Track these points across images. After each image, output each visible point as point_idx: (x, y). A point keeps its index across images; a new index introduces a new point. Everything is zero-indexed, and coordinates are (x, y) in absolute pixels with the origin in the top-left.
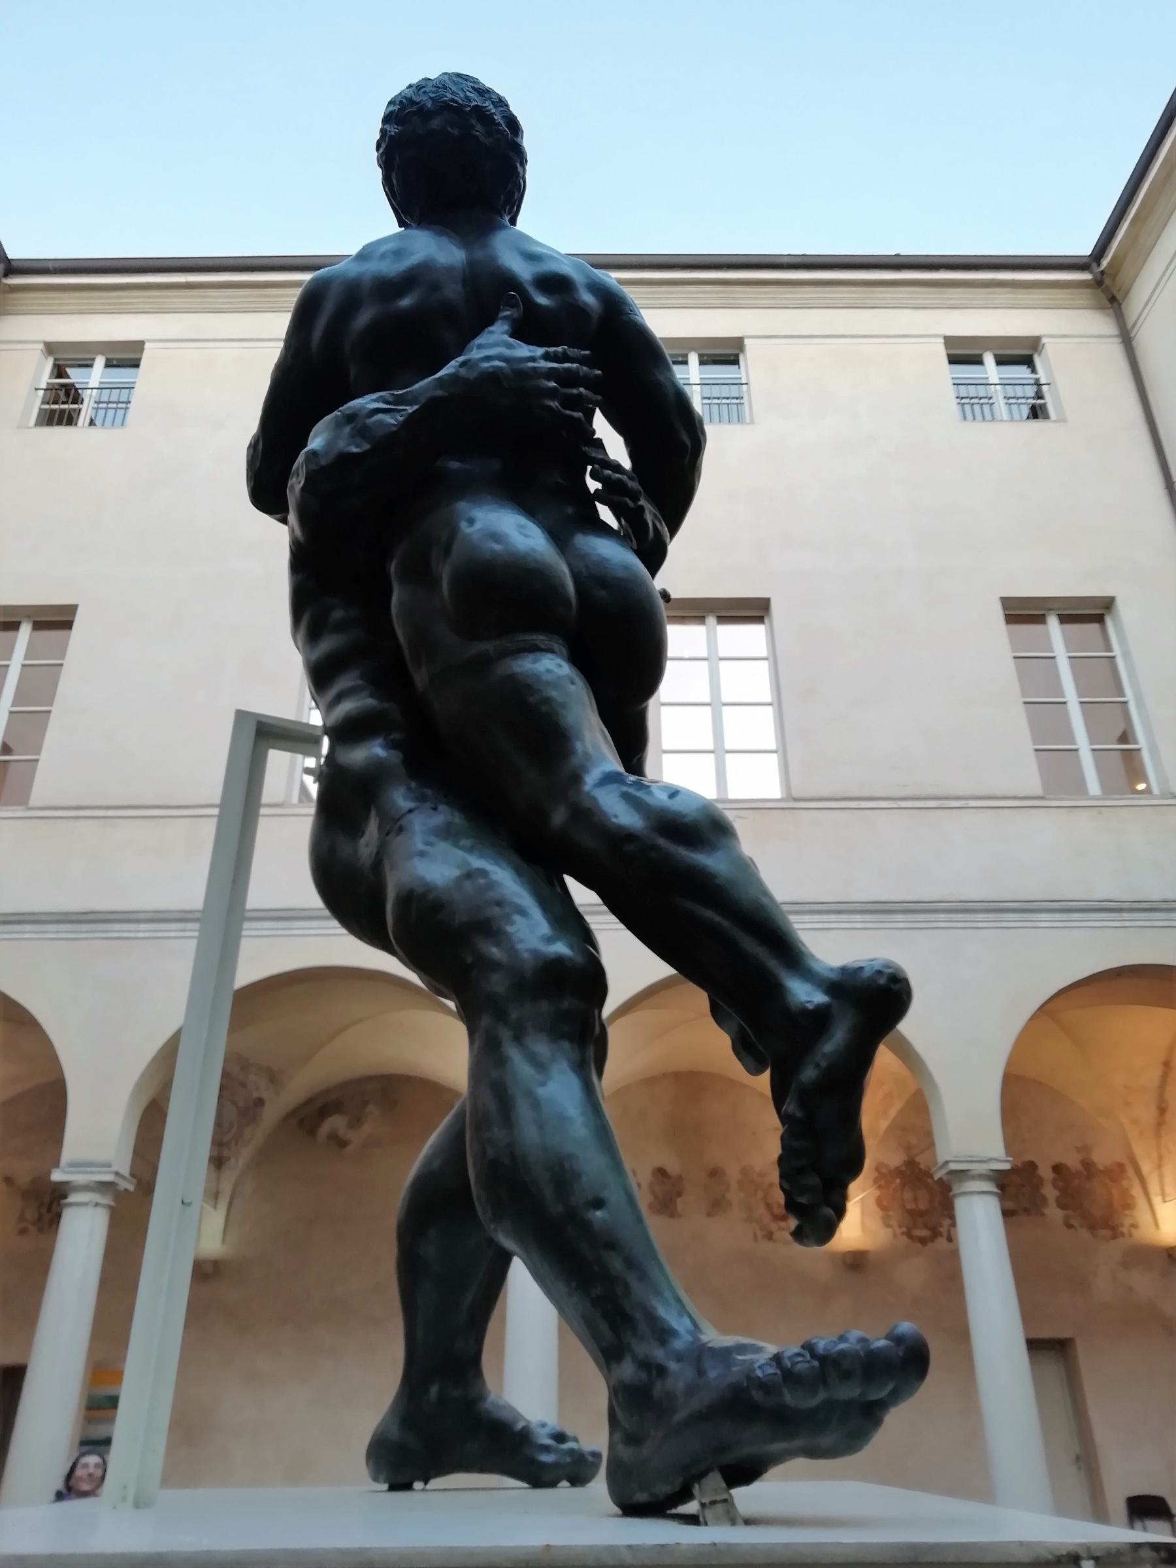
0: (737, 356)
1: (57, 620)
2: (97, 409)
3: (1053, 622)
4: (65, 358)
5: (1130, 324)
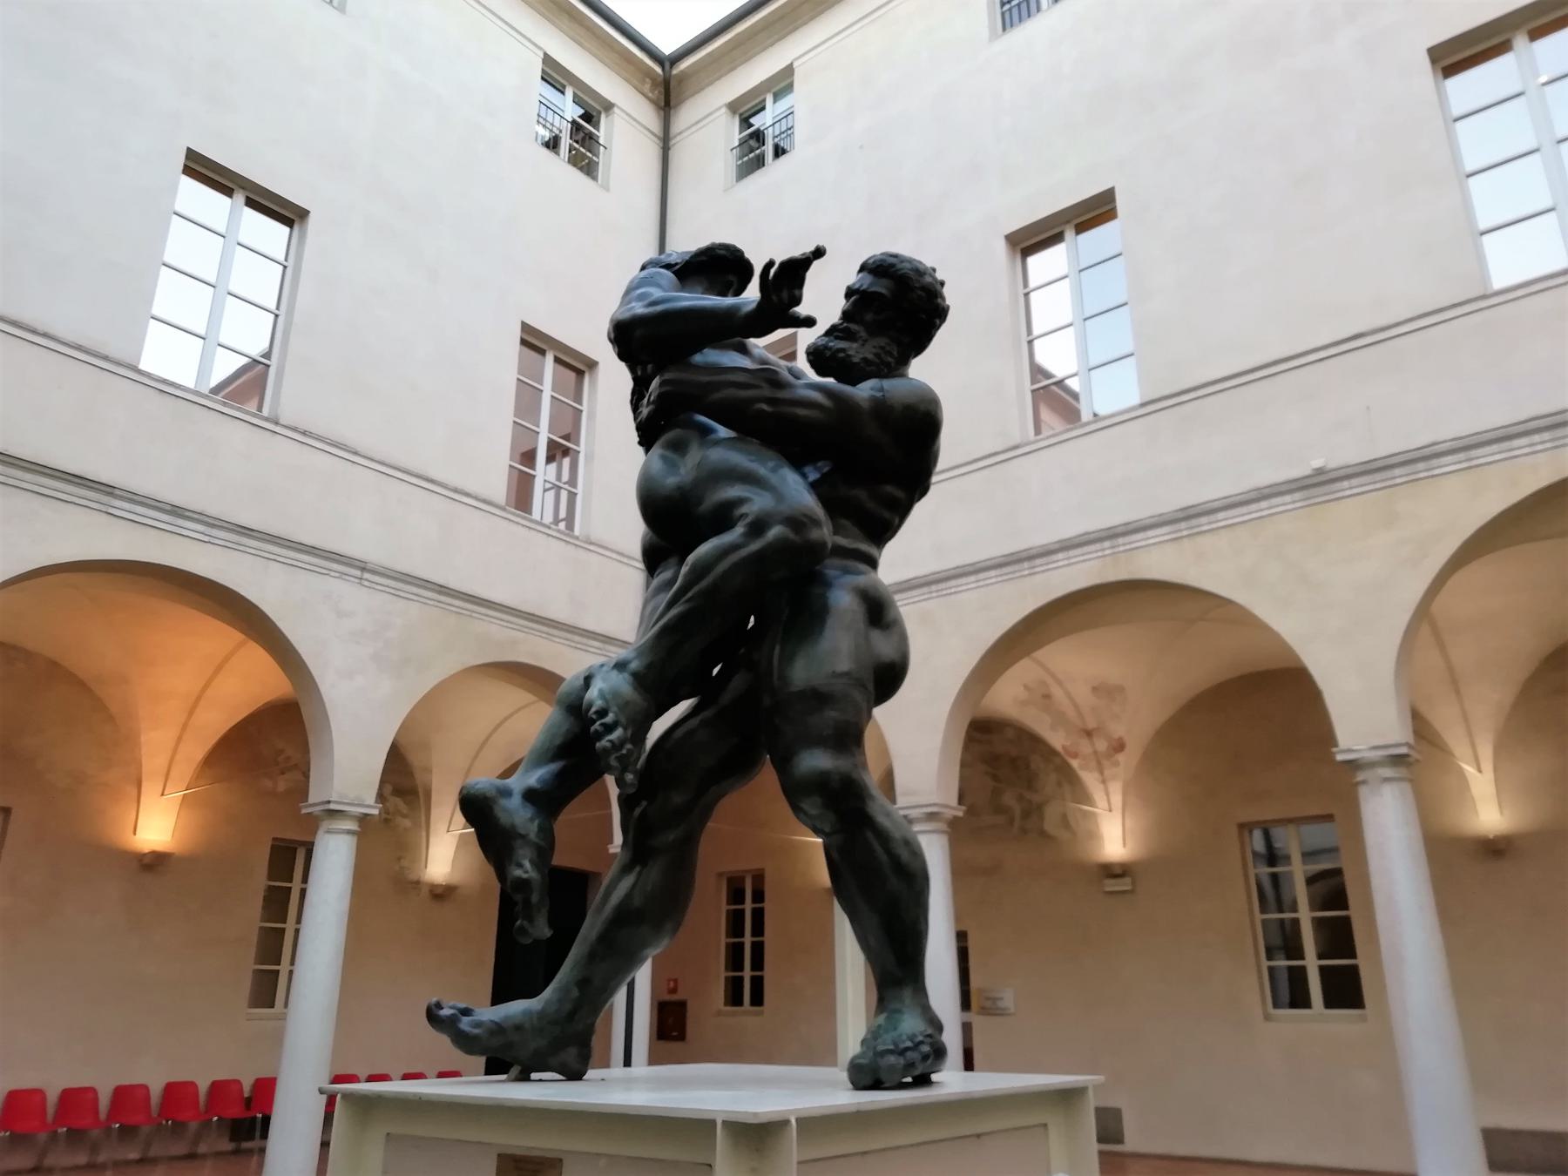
5: (674, 129)
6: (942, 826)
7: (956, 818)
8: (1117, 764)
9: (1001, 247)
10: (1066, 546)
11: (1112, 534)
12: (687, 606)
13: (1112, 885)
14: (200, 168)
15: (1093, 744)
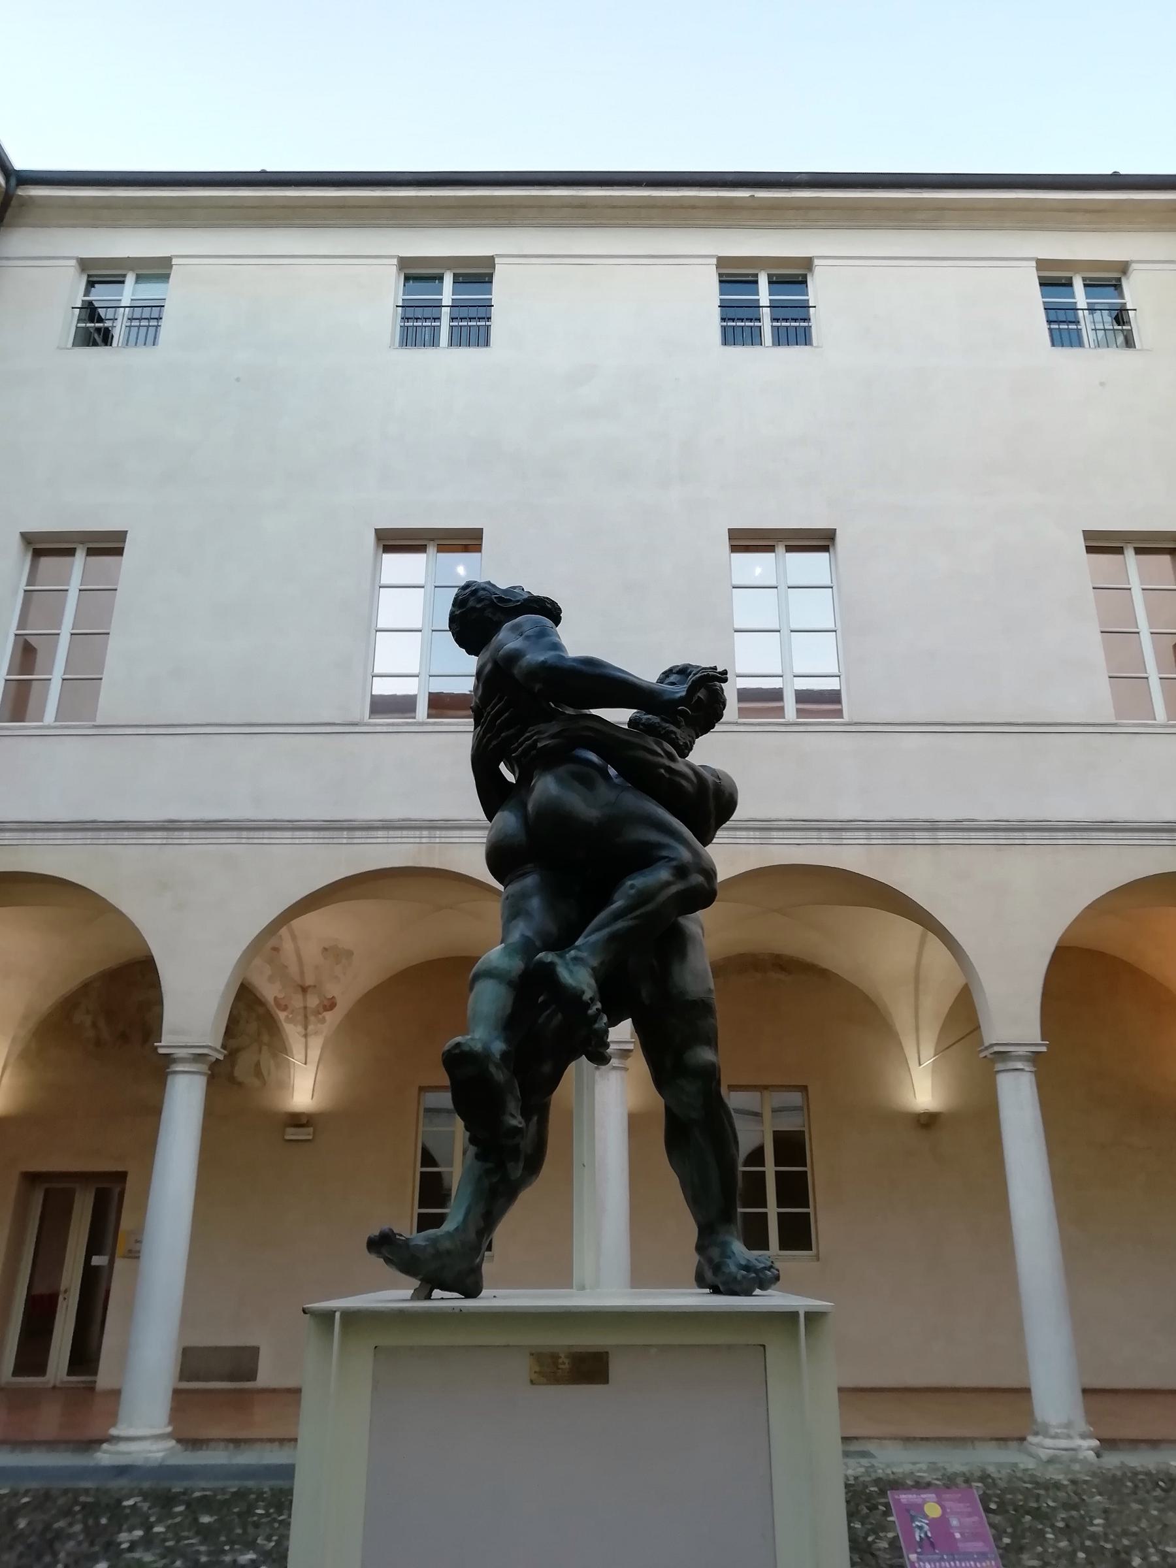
0: (805, 276)
1: (108, 545)
2: (130, 326)
3: (1130, 553)
4: (99, 274)
6: (204, 1068)
8: (323, 1021)
10: (388, 826)
11: (432, 826)
12: (630, 923)
13: (292, 1134)
14: (747, 541)
15: (305, 1000)
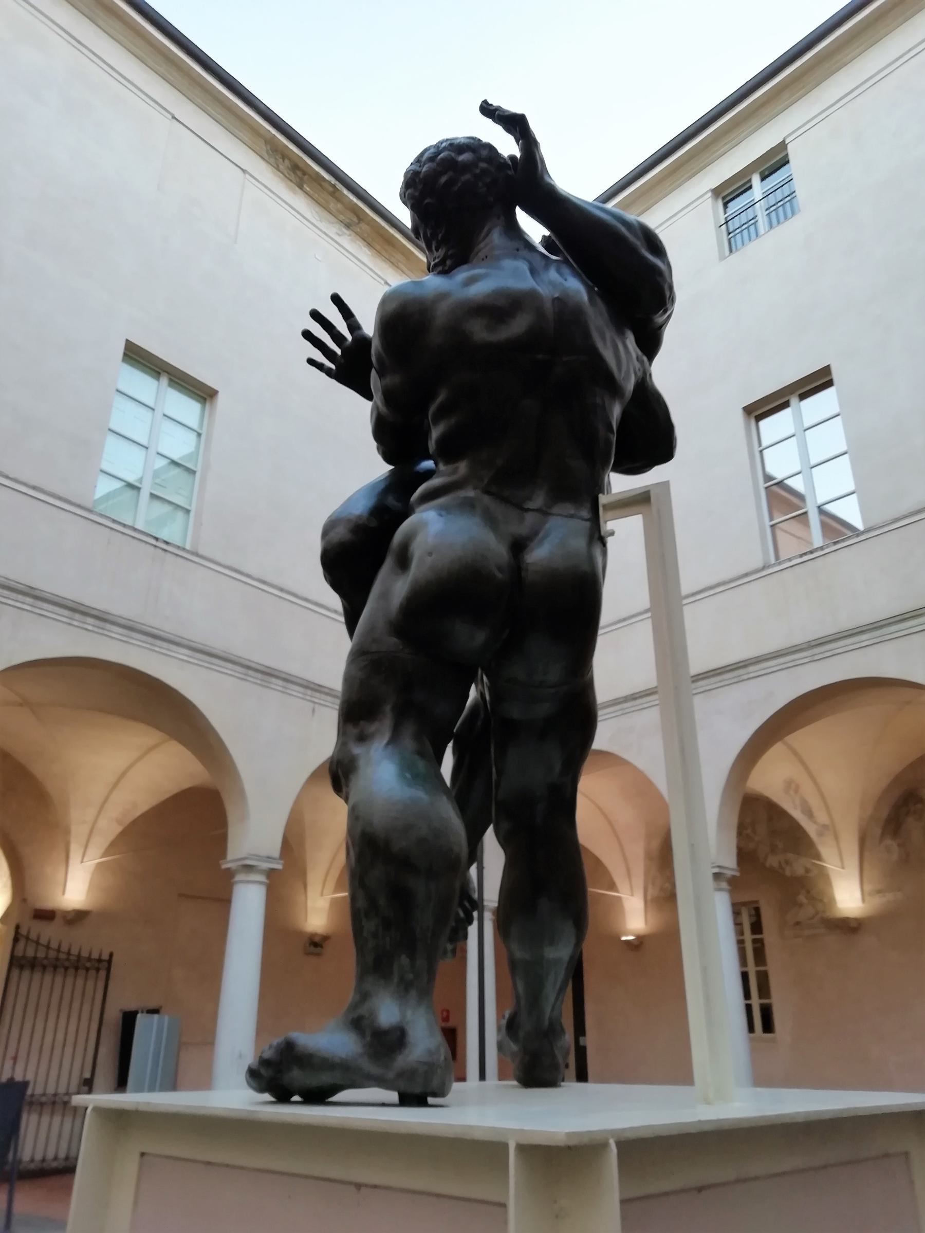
7: (734, 876)
9: (739, 416)
